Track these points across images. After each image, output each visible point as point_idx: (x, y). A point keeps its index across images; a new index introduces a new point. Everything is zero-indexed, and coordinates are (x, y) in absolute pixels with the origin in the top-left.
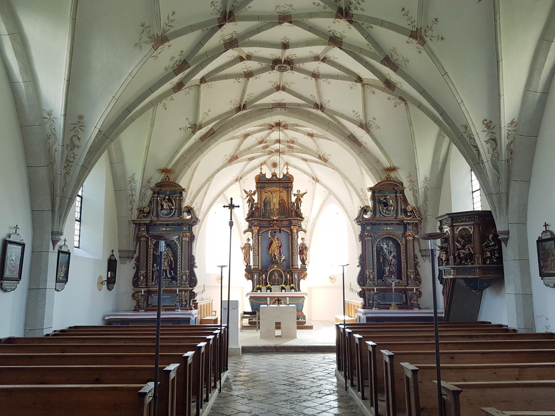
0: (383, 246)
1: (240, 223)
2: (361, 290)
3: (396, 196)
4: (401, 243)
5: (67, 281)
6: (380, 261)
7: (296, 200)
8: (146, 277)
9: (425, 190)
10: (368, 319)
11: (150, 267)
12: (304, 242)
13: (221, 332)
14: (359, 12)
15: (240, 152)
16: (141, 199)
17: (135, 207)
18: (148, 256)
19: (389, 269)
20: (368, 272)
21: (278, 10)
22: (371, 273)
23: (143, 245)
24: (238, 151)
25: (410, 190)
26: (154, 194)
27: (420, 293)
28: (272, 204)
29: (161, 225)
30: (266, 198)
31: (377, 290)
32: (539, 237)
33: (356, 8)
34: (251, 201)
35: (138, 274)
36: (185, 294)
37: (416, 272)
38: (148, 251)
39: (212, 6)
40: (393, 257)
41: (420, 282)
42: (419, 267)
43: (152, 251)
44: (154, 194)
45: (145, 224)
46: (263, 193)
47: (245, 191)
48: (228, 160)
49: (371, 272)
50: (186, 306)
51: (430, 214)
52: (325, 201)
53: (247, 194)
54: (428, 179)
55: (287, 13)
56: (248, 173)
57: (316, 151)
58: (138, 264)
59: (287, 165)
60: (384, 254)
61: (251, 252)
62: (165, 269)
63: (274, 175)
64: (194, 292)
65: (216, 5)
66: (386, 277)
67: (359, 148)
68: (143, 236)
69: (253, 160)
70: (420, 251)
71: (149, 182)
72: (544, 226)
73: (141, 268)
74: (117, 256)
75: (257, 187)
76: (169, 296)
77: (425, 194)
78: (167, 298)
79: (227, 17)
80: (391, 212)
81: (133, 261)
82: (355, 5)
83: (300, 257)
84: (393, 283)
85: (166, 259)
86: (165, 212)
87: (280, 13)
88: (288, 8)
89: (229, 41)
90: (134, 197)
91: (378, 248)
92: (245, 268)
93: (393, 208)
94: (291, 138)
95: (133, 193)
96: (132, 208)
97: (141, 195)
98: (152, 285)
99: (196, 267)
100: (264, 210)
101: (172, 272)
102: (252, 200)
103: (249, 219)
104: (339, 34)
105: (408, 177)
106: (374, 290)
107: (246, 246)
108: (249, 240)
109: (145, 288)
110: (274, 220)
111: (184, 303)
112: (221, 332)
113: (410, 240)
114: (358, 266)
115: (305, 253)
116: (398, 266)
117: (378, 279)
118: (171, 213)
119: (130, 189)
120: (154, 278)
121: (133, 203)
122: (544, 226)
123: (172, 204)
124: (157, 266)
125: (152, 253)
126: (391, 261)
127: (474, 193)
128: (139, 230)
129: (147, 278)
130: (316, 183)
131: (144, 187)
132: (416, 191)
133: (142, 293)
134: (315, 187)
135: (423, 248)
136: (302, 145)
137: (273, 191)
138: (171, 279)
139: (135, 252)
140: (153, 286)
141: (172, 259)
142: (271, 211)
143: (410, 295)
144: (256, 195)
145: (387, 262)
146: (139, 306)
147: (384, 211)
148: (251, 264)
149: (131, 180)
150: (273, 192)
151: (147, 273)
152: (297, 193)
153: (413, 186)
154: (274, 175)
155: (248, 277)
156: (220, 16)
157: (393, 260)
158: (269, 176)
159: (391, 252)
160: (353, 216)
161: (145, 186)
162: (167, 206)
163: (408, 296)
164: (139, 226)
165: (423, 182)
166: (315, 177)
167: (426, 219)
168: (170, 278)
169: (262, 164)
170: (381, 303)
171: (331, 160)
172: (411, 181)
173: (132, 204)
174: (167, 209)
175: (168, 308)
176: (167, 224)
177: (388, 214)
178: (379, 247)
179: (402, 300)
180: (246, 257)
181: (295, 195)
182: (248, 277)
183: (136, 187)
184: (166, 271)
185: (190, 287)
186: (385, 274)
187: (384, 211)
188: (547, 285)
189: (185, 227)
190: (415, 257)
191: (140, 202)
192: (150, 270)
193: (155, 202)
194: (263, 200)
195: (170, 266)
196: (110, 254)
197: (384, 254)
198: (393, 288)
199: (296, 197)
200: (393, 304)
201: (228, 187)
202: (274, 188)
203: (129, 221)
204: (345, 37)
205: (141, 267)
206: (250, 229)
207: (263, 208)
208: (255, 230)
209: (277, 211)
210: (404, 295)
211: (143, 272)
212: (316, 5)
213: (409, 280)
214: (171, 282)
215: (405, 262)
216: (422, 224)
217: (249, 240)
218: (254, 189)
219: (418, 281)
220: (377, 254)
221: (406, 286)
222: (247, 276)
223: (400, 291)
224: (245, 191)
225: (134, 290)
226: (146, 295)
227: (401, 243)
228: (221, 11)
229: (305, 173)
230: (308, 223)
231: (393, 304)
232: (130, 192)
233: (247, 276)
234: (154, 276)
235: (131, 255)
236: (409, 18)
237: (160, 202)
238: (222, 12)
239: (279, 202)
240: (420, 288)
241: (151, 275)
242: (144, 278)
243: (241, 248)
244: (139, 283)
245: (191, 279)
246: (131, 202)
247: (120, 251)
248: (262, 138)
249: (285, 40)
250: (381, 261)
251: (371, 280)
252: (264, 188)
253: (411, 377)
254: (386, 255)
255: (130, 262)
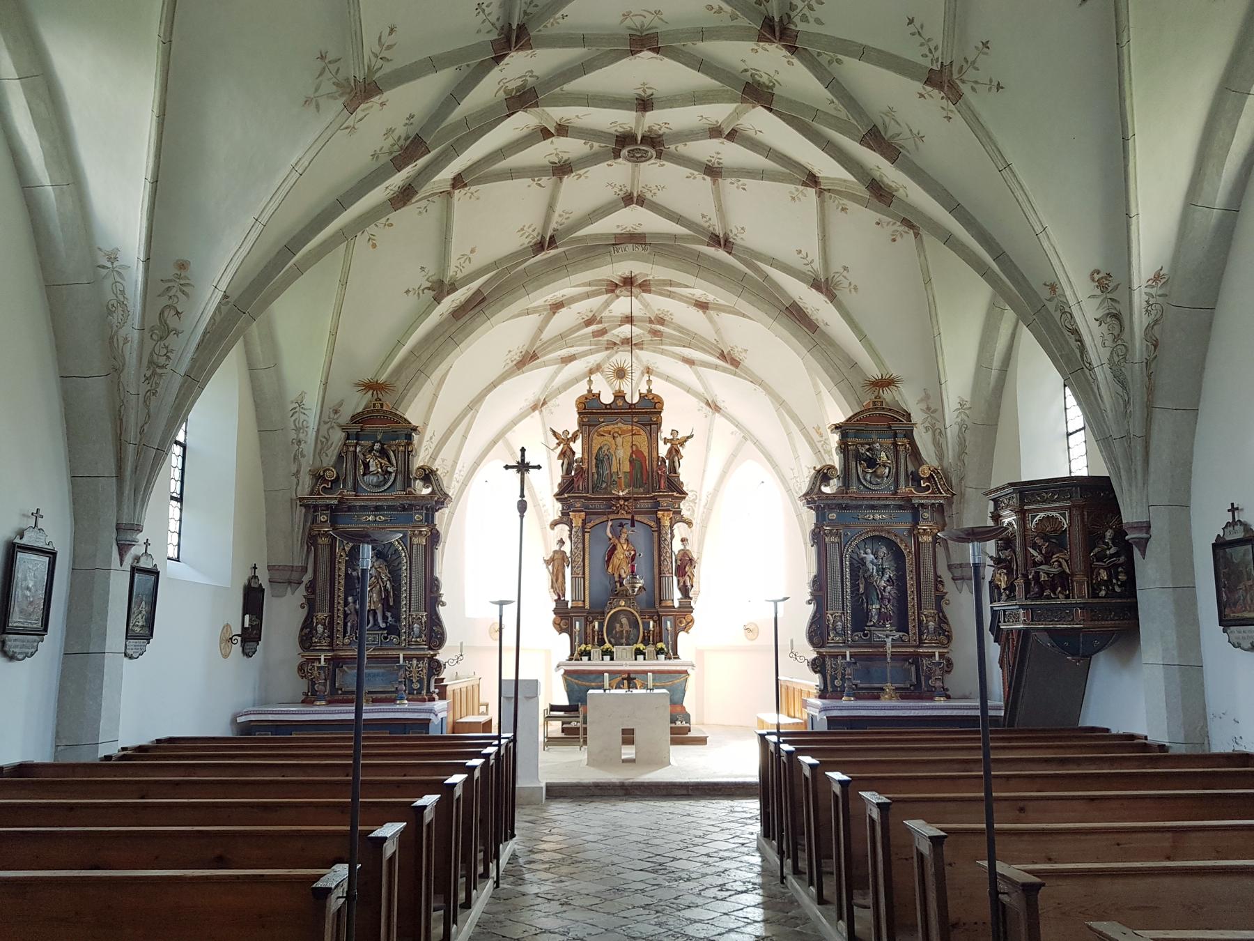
0: (865, 555)
1: (541, 505)
2: (815, 655)
3: (895, 444)
4: (905, 549)
5: (152, 635)
6: (858, 590)
7: (670, 452)
8: (330, 626)
9: (960, 429)
10: (831, 721)
11: (339, 603)
12: (687, 548)
13: (499, 750)
14: (811, 27)
15: (542, 345)
16: (318, 451)
17: (305, 469)
18: (335, 578)
19: (880, 609)
20: (832, 615)
21: (628, 22)
22: (838, 618)
23: (324, 554)
24: (539, 342)
25: (927, 429)
26: (348, 439)
27: (950, 663)
28: (614, 462)
29: (364, 508)
30: (600, 448)
31: (851, 656)
32: (1219, 535)
33: (805, 19)
34: (566, 454)
35: (312, 621)
36: (417, 665)
37: (941, 614)
38: (335, 567)
39: (479, 13)
40: (888, 581)
41: (949, 638)
42: (946, 603)
43: (343, 569)
44: (348, 439)
45: (328, 507)
46: (595, 436)
47: (554, 433)
48: (515, 362)
49: (839, 614)
50: (419, 691)
51: (971, 485)
52: (734, 455)
53: (558, 439)
54: (968, 405)
55: (648, 30)
56: (560, 391)
57: (715, 342)
58: (313, 597)
59: (648, 373)
60: (868, 574)
61: (568, 571)
62: (373, 608)
63: (619, 395)
64: (438, 661)
65: (487, 10)
66: (872, 626)
67: (811, 334)
68: (323, 534)
69: (571, 361)
70: (950, 567)
71: (336, 412)
72: (1229, 511)
73: (318, 605)
74: (264, 580)
75: (581, 424)
76: (381, 671)
77: (959, 438)
78: (378, 675)
79: (514, 39)
80: (883, 480)
81: (301, 591)
82: (803, 12)
83: (678, 581)
84: (889, 641)
85: (375, 586)
86: (373, 479)
87: (632, 29)
88: (650, 17)
89: (518, 94)
90: (303, 445)
91: (855, 562)
92: (553, 605)
93: (887, 470)
94: (657, 312)
95: (301, 436)
96: (298, 472)
97: (319, 442)
98: (343, 644)
99: (443, 604)
100: (596, 476)
101: (389, 614)
102: (568, 452)
103: (563, 496)
104: (765, 77)
105: (921, 401)
106: (844, 656)
107: (556, 556)
108: (564, 543)
109: (329, 651)
110: (619, 498)
111: (416, 686)
112: (499, 750)
113: (926, 542)
114: (809, 602)
115: (689, 573)
116: (898, 601)
117: (853, 632)
118: (386, 481)
119: (293, 427)
120: (349, 629)
121: (301, 459)
122: (1229, 511)
123: (389, 460)
124: (354, 602)
125: (342, 573)
126: (884, 590)
127: (1070, 437)
128: (314, 521)
129: (333, 629)
130: (713, 414)
131: (326, 423)
132: (941, 432)
133: (320, 663)
134: (711, 424)
135: (956, 560)
136: (683, 328)
137: (617, 432)
138: (386, 632)
139: (304, 570)
140: (345, 647)
141: (388, 586)
142: (612, 477)
143: (927, 667)
144: (579, 441)
145: (875, 593)
146: (314, 693)
147: (868, 478)
148: (568, 597)
149: (295, 408)
150: (616, 435)
151: (332, 617)
152: (671, 437)
153: (934, 421)
154: (619, 395)
155: (560, 627)
156: (497, 37)
157: (889, 588)
158: (607, 398)
159: (884, 569)
160: (797, 489)
161: (328, 420)
162: (377, 465)
163: (923, 670)
164: (314, 512)
165: (957, 413)
166: (713, 401)
167: (962, 495)
168: (384, 629)
169: (591, 372)
170: (861, 685)
171: (748, 362)
172: (928, 409)
173: (299, 461)
174: (378, 472)
175: (380, 696)
176: (377, 506)
177: (878, 484)
178: (857, 559)
179: (908, 678)
180: (557, 580)
181: (666, 441)
182: (560, 627)
183: (307, 422)
184: (375, 612)
185: (430, 649)
186: (871, 621)
187: (868, 478)
188: (1236, 646)
189: (418, 513)
190: (938, 581)
191: (317, 456)
192: (338, 610)
193: (350, 456)
194: (595, 452)
195: (385, 601)
196: (249, 573)
197: (868, 574)
198: (889, 652)
199: (669, 445)
200: (889, 687)
201: (514, 422)
202: (620, 425)
203: (291, 499)
204: (779, 83)
205: (318, 605)
206: (565, 518)
207: (594, 470)
208: (577, 521)
209: (625, 477)
210: (913, 668)
211: (322, 615)
212: (714, 11)
213: (924, 633)
214: (386, 638)
215: (915, 592)
216: (954, 506)
217: (562, 542)
218: (573, 427)
219: (944, 635)
220: (851, 575)
221: (918, 647)
222: (559, 624)
223: (905, 657)
224: (554, 433)
225: (303, 656)
226: (331, 667)
227: (905, 549)
228: (499, 25)
229: (688, 392)
230: (697, 505)
231: (889, 687)
232: (293, 435)
233: (559, 624)
234: (349, 624)
235: (295, 576)
236: (923, 41)
237: (361, 456)
238: (502, 28)
239: (631, 456)
240: (948, 652)
241: (341, 623)
242: (325, 629)
243: (545, 560)
244: (315, 640)
245: (431, 630)
246: (295, 458)
247: (270, 568)
248: (591, 311)
249: (644, 91)
250: (861, 591)
251: (837, 634)
252: (596, 425)
253: (928, 853)
254: (871, 576)
255: (293, 593)
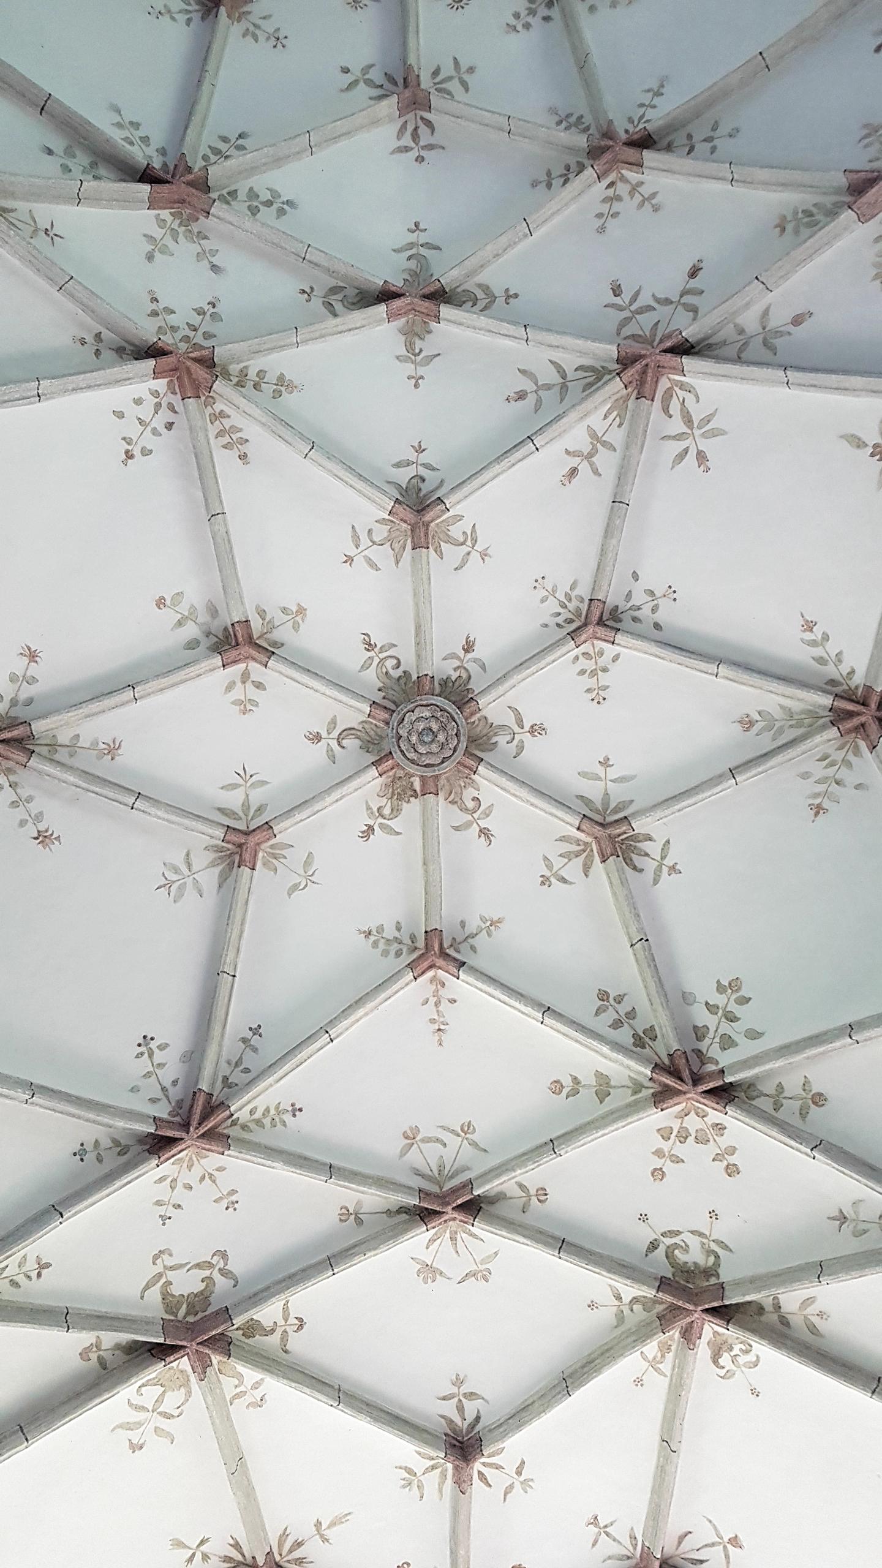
14: (746, 1049)
21: (414, 1157)
33: (727, 1043)
39: (142, 1054)
55: (452, 1177)
65: (159, 1056)
79: (196, 1118)
82: (721, 1031)
87: (423, 1176)
88: (453, 1142)
89: (191, 1319)
104: (694, 1242)
156: (165, 1116)
204: (726, 1247)
212: (565, 1091)
228: (175, 1093)
238: (180, 1104)
249: (460, 1409)
